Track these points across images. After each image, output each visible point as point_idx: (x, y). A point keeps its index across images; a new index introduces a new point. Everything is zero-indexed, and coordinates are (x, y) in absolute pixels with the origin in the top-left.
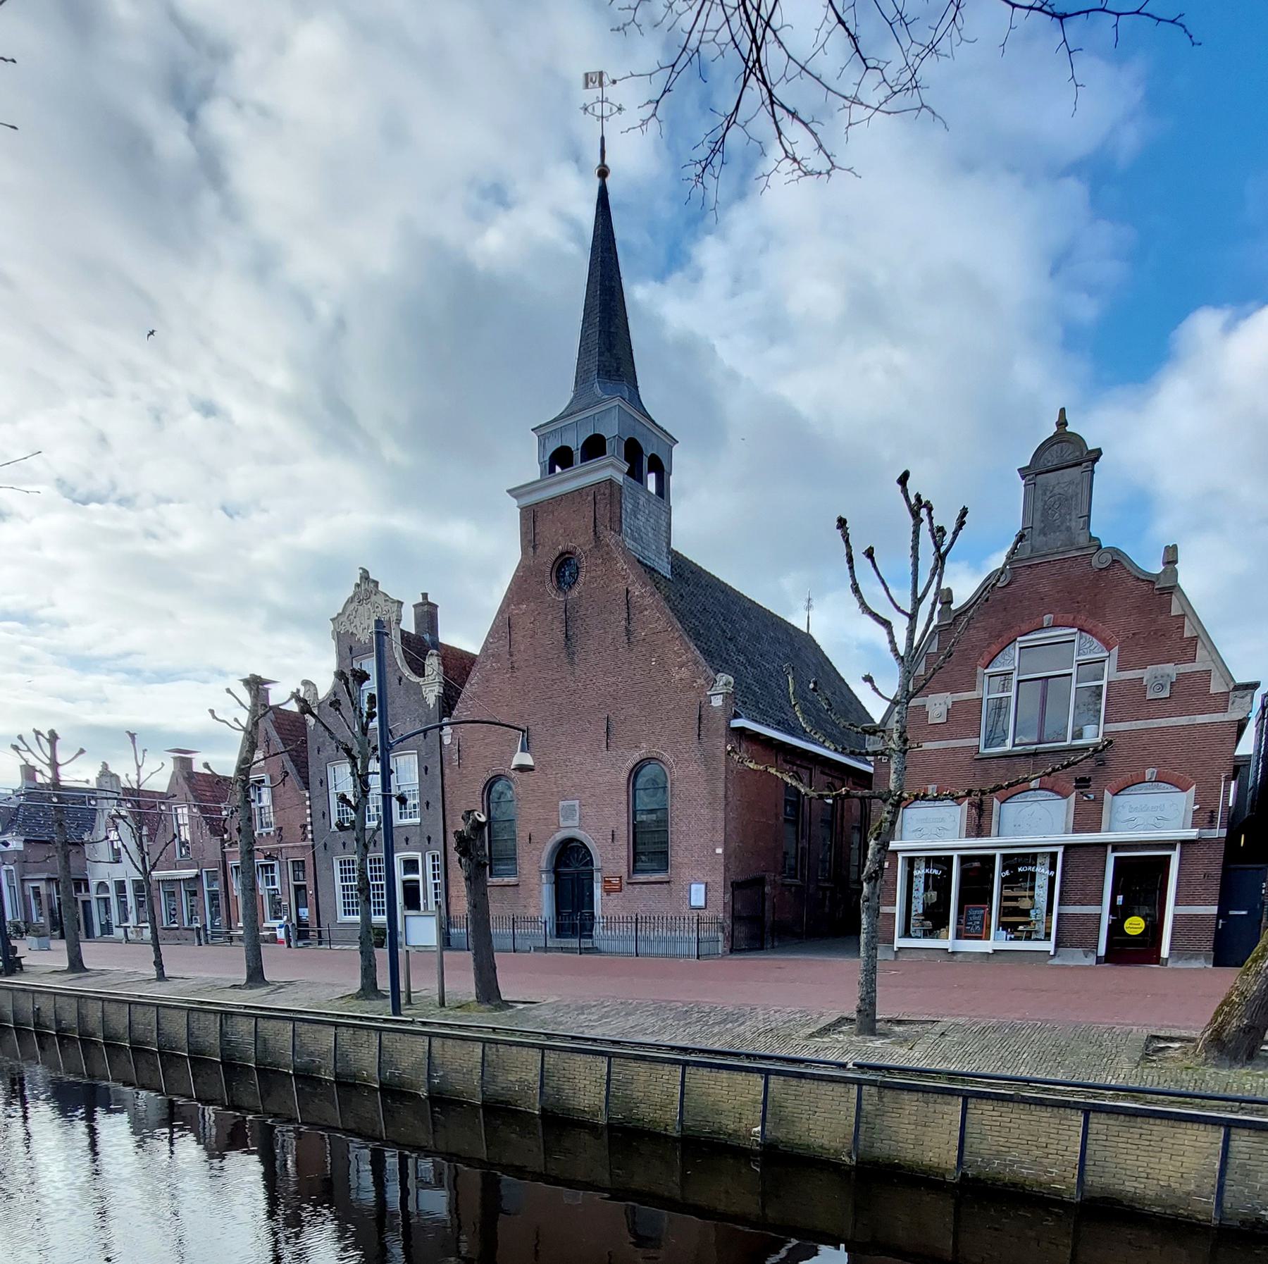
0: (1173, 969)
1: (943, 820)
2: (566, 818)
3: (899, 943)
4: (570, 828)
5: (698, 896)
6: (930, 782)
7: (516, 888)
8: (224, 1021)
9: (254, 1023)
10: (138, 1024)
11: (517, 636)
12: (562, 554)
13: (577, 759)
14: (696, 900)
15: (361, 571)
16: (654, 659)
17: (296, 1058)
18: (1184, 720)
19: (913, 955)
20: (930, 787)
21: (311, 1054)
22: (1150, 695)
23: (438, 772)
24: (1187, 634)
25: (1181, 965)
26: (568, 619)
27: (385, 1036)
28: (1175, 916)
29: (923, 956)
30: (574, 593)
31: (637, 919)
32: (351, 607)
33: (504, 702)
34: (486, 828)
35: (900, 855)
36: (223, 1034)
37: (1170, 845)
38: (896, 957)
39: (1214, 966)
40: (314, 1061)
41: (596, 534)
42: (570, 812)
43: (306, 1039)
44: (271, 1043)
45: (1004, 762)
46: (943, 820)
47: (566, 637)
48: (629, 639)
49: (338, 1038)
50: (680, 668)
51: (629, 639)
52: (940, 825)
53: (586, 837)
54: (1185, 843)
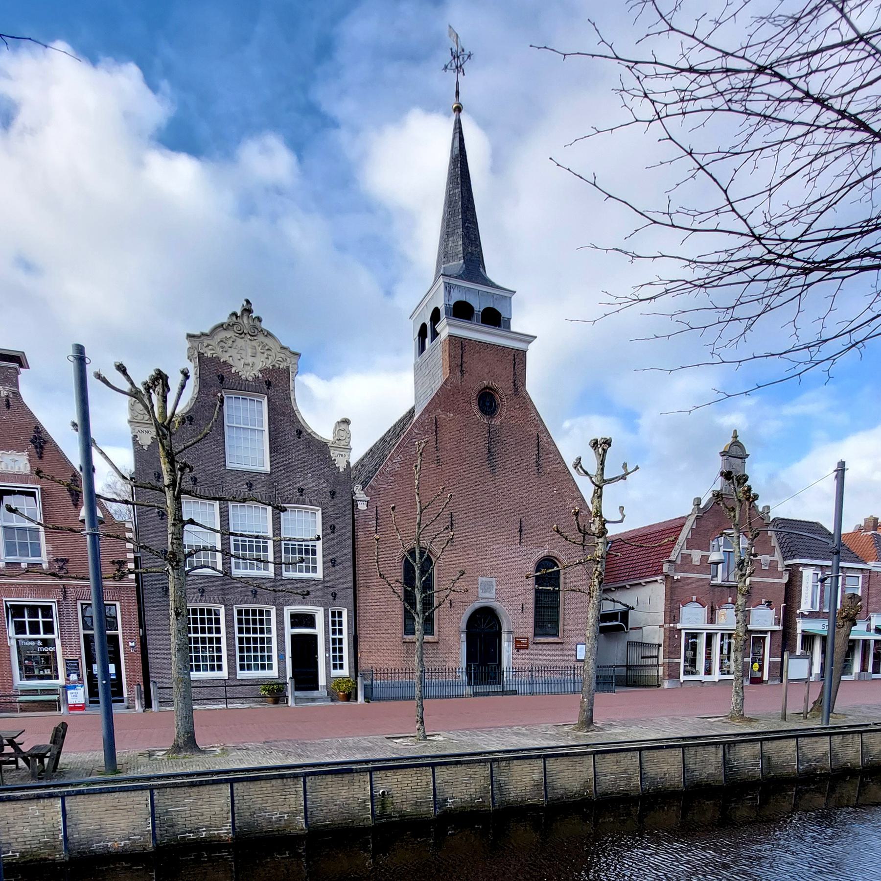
0: (770, 685)
1: (697, 614)
2: (485, 591)
3: (683, 678)
4: (487, 597)
5: (581, 652)
6: (693, 594)
7: (434, 646)
8: (727, 750)
9: (301, 790)
10: (606, 775)
11: (445, 435)
12: (486, 388)
13: (496, 546)
14: (580, 655)
15: (245, 303)
16: (555, 489)
17: (799, 766)
18: (771, 580)
19: (688, 684)
20: (694, 597)
21: (809, 761)
22: (763, 568)
23: (349, 533)
24: (772, 545)
25: (772, 683)
26: (492, 437)
27: (865, 736)
28: (770, 662)
29: (692, 684)
30: (496, 422)
31: (574, 668)
32: (223, 334)
33: (429, 487)
34: (839, 607)
35: (683, 632)
36: (726, 762)
37: (765, 632)
38: (681, 685)
39: (750, 683)
40: (811, 765)
41: (515, 385)
42: (487, 587)
43: (806, 749)
44: (774, 759)
45: (720, 589)
46: (697, 614)
47: (489, 452)
48: (538, 470)
49: (832, 744)
50: (573, 500)
51: (538, 470)
52: (697, 617)
53: (501, 607)
54: (772, 632)
